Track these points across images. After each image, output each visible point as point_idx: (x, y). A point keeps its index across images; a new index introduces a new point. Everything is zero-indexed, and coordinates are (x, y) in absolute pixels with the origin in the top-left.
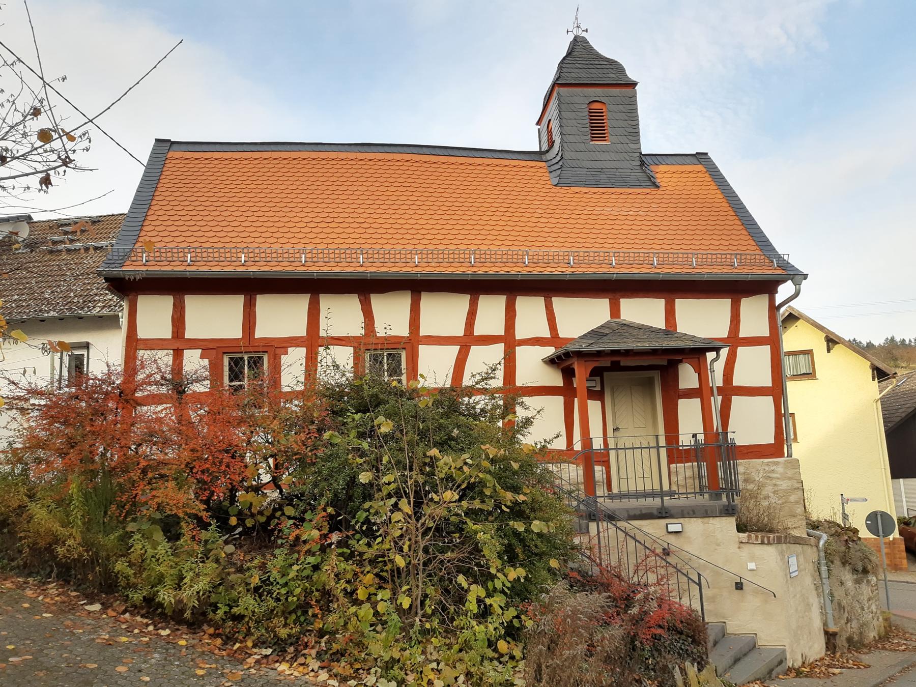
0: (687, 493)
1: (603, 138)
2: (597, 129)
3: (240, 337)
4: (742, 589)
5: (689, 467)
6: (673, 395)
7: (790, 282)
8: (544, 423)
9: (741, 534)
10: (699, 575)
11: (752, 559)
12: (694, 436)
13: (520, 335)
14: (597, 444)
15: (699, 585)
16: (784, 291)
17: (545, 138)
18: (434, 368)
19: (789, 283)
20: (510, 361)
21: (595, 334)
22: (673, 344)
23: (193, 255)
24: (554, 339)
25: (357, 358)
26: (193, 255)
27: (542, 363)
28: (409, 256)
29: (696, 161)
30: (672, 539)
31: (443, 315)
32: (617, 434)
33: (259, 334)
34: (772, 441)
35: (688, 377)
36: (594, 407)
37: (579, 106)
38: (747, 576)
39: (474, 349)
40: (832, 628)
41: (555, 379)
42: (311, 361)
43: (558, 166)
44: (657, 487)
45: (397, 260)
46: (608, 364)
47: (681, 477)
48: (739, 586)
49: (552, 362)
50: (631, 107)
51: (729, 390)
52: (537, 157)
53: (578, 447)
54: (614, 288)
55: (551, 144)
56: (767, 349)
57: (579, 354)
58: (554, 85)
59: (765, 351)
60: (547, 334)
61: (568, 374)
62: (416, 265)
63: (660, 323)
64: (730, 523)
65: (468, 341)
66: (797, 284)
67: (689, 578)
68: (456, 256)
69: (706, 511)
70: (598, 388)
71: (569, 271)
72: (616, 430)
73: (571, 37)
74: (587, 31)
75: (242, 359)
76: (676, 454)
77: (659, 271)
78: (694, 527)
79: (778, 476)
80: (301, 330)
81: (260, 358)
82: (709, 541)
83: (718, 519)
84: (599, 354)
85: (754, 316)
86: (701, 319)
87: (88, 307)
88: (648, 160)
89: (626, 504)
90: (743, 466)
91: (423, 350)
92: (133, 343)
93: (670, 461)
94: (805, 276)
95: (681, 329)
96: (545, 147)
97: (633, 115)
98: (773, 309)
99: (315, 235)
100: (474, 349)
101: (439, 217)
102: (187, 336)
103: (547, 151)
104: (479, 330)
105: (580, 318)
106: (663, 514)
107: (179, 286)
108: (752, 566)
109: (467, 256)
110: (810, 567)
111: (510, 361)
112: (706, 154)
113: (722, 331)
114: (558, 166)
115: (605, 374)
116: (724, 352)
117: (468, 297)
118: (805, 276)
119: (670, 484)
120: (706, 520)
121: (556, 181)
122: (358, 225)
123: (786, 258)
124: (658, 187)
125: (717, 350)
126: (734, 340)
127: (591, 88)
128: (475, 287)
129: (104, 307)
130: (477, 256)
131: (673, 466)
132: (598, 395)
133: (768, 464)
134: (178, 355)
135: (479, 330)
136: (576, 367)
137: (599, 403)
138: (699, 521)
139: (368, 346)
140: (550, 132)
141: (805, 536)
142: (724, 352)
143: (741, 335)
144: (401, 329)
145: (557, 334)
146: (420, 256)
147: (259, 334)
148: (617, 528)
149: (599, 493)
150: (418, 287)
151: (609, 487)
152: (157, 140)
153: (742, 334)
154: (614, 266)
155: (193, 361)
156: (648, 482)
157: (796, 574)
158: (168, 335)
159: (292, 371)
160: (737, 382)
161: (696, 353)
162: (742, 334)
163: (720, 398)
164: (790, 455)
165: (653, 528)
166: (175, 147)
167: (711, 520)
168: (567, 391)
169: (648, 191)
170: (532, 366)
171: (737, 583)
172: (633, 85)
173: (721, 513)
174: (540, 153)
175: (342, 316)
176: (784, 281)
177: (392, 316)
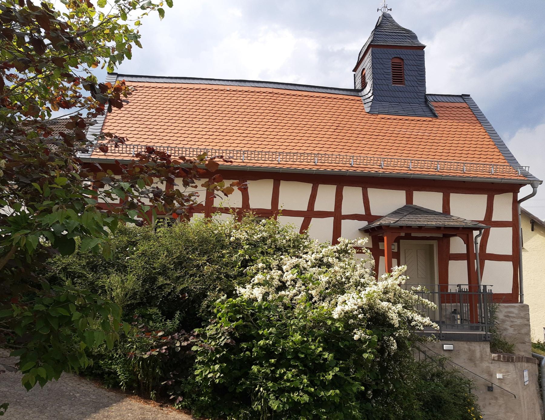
1: (401, 82)
4: (492, 391)
6: (446, 257)
12: (459, 286)
13: (344, 212)
17: (359, 81)
19: (529, 187)
20: (210, 197)
24: (368, 216)
27: (358, 231)
29: (462, 100)
31: (295, 197)
35: (457, 245)
39: (313, 220)
45: (274, 159)
49: (365, 231)
51: (485, 256)
56: (510, 230)
57: (388, 228)
60: (362, 212)
65: (309, 215)
66: (534, 187)
71: (381, 171)
73: (380, 14)
74: (391, 10)
86: (467, 209)
88: (430, 98)
96: (359, 87)
97: (421, 68)
99: (198, 140)
100: (313, 220)
101: (286, 131)
104: (317, 207)
105: (386, 203)
111: (210, 197)
112: (469, 95)
113: (481, 216)
117: (312, 185)
118: (541, 182)
126: (489, 222)
128: (315, 179)
135: (317, 207)
140: (363, 77)
145: (370, 213)
153: (494, 219)
161: (465, 231)
162: (494, 219)
164: (522, 302)
168: (376, 252)
174: (355, 90)
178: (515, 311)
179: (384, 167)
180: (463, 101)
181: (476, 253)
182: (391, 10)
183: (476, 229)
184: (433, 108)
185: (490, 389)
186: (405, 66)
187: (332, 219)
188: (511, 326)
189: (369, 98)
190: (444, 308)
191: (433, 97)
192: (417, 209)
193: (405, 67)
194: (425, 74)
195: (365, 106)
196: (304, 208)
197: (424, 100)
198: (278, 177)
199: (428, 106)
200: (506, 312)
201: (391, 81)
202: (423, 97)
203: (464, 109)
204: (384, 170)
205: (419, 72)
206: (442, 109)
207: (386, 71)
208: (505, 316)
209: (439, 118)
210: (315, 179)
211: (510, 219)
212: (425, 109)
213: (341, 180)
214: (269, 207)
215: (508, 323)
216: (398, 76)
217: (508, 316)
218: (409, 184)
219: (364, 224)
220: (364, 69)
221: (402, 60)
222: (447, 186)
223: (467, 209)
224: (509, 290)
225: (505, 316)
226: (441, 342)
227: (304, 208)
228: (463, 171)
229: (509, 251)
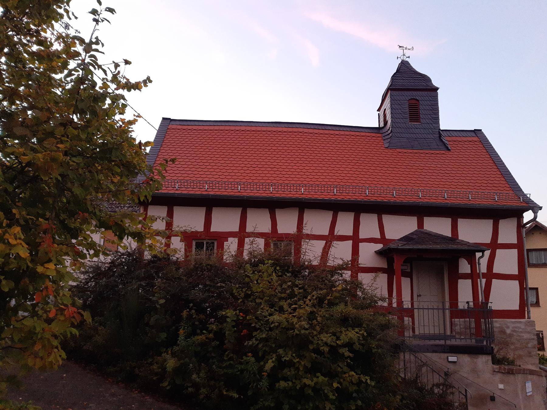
2: (414, 116)
3: (203, 230)
4: (494, 400)
6: (455, 276)
7: (530, 211)
8: (375, 285)
10: (466, 390)
12: (468, 303)
13: (362, 236)
14: (407, 305)
16: (528, 216)
19: (530, 212)
20: (355, 251)
21: (407, 239)
22: (455, 247)
23: (180, 184)
24: (383, 239)
25: (267, 245)
26: (180, 184)
28: (298, 188)
30: (451, 367)
31: (317, 223)
32: (419, 298)
33: (213, 229)
34: (517, 308)
35: (464, 267)
36: (405, 282)
37: (402, 102)
38: (497, 394)
41: (382, 264)
42: (241, 245)
43: (389, 137)
44: (442, 332)
50: (433, 102)
51: (490, 275)
52: (376, 131)
53: (395, 305)
54: (420, 211)
55: (386, 123)
56: (515, 251)
58: (388, 90)
59: (514, 252)
60: (378, 236)
61: (390, 262)
62: (303, 193)
63: (447, 232)
64: (489, 358)
65: (331, 238)
68: (326, 189)
70: (409, 270)
72: (419, 296)
73: (399, 61)
74: (409, 57)
77: (448, 201)
79: (521, 330)
80: (235, 227)
81: (213, 243)
85: (508, 233)
86: (474, 232)
87: (121, 207)
89: (421, 343)
90: (498, 323)
93: (452, 317)
94: (541, 208)
95: (460, 238)
96: (382, 125)
97: (436, 107)
103: (383, 128)
105: (399, 228)
107: (171, 202)
109: (332, 189)
111: (355, 251)
112: (481, 130)
113: (487, 239)
116: (487, 253)
117: (332, 212)
118: (541, 208)
121: (387, 145)
122: (271, 169)
123: (528, 196)
124: (449, 150)
125: (483, 251)
127: (411, 92)
128: (335, 207)
129: (129, 207)
130: (338, 189)
132: (409, 275)
136: (395, 257)
139: (273, 237)
141: (538, 369)
142: (487, 253)
143: (499, 242)
146: (305, 188)
147: (213, 229)
149: (406, 334)
150: (302, 206)
152: (164, 119)
153: (500, 241)
154: (421, 196)
155: (177, 243)
156: (432, 328)
157: (531, 394)
160: (496, 270)
161: (470, 252)
162: (500, 241)
163: (484, 281)
164: (529, 318)
165: (437, 359)
166: (172, 123)
168: (389, 271)
169: (444, 152)
170: (368, 254)
171: (491, 397)
172: (437, 89)
175: (259, 222)
177: (287, 224)
181: (479, 273)
182: (409, 57)
183: (479, 251)
184: (446, 142)
185: (493, 399)
186: (421, 106)
187: (351, 242)
189: (389, 134)
191: (448, 132)
192: (426, 233)
194: (438, 113)
195: (385, 142)
196: (499, 252)
197: (438, 135)
199: (442, 141)
200: (513, 327)
201: (408, 120)
203: (476, 143)
206: (455, 143)
209: (452, 151)
211: (515, 242)
218: (420, 211)
220: (385, 109)
223: (474, 232)
224: (515, 306)
226: (446, 355)
227: (326, 233)
228: (469, 198)
229: (515, 271)
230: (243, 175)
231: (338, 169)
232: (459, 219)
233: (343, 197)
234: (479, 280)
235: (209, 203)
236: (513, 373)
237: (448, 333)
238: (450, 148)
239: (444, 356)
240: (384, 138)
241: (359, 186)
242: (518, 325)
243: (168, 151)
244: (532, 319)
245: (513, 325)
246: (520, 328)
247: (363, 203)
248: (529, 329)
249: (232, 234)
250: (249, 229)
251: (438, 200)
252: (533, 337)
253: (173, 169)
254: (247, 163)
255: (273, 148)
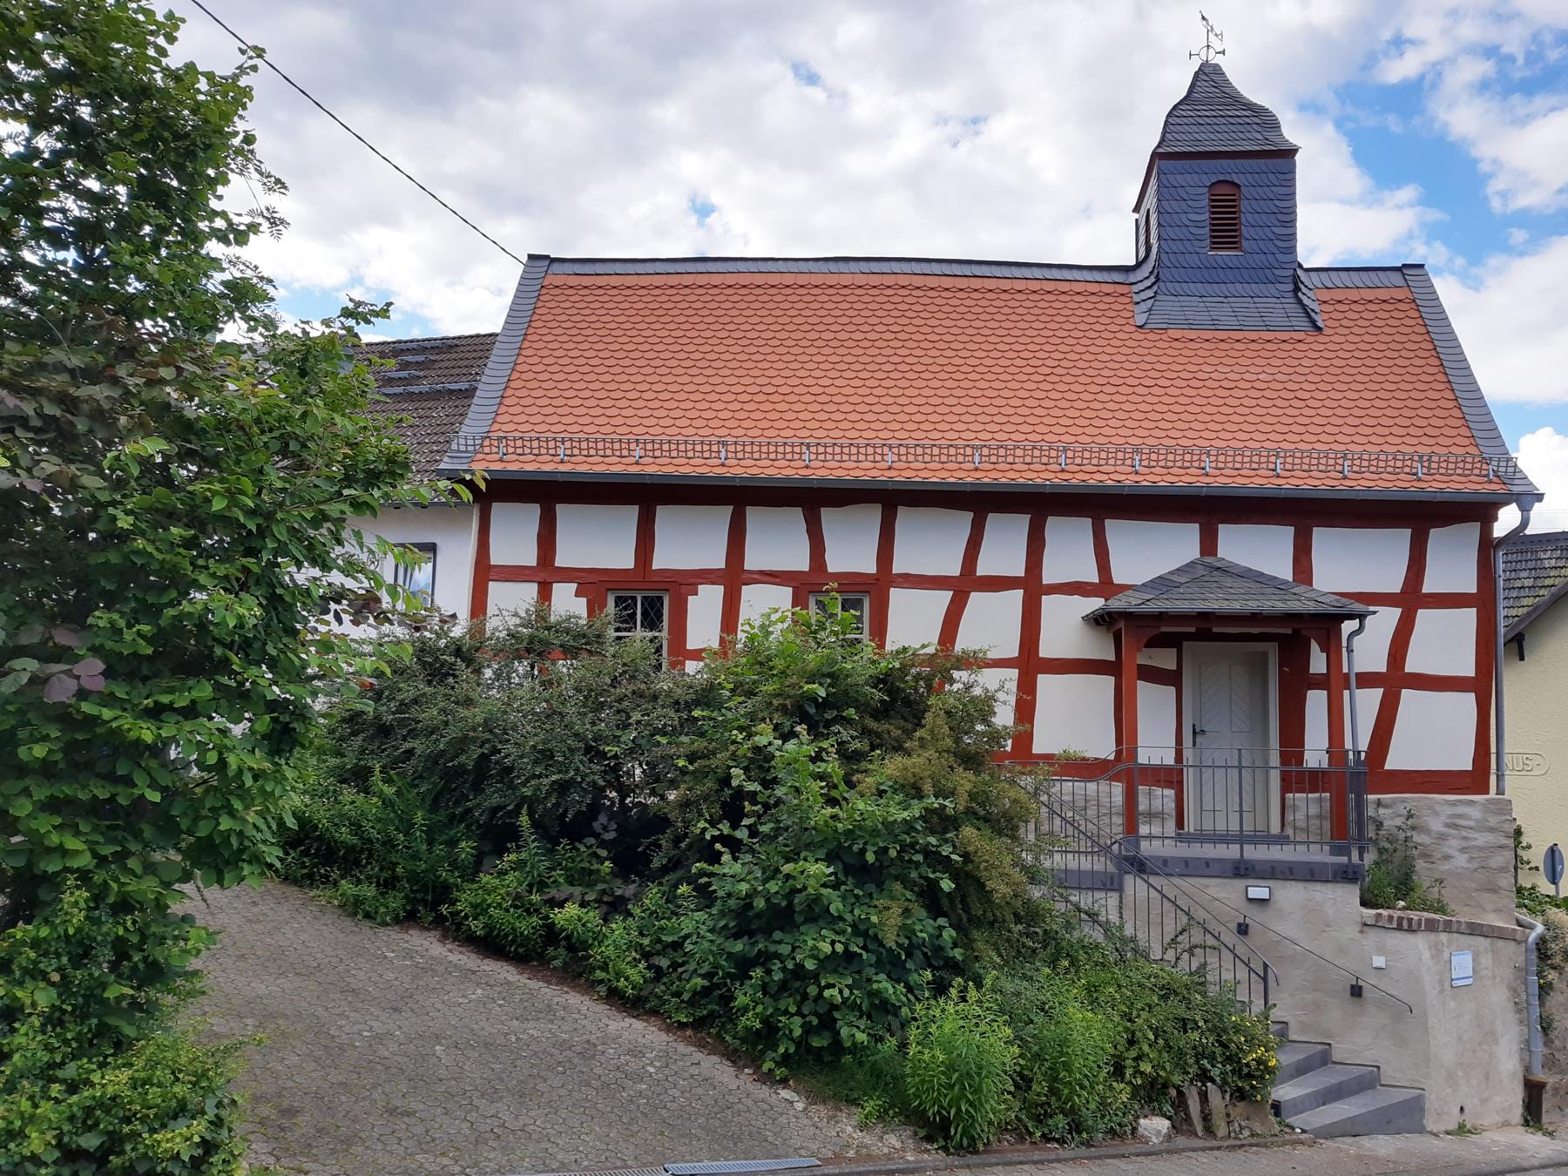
0: (1308, 843)
1: (1234, 244)
5: (1314, 800)
6: (1296, 685)
8: (1072, 718)
9: (1365, 911)
10: (1266, 966)
11: (1381, 951)
13: (1048, 578)
15: (1265, 979)
16: (1507, 520)
18: (913, 622)
31: (931, 546)
33: (658, 563)
38: (1369, 981)
39: (975, 597)
40: (1539, 1075)
41: (1100, 648)
43: (1150, 293)
46: (1193, 630)
47: (1300, 815)
48: (1356, 991)
49: (1099, 620)
51: (1395, 680)
54: (1209, 510)
56: (1470, 614)
59: (1468, 618)
60: (1093, 577)
65: (964, 585)
67: (1251, 969)
69: (1312, 871)
75: (634, 599)
76: (1297, 778)
78: (1291, 894)
79: (1472, 823)
80: (718, 561)
81: (660, 599)
82: (1318, 920)
83: (1329, 886)
84: (1162, 617)
85: (1452, 564)
86: (1353, 564)
91: (897, 596)
92: (485, 572)
93: (1286, 787)
98: (1488, 546)
102: (557, 564)
104: (984, 568)
105: (1149, 557)
106: (1242, 870)
108: (1379, 961)
110: (1508, 973)
112: (1422, 266)
113: (1393, 582)
114: (1150, 293)
115: (1185, 644)
117: (969, 516)
119: (1283, 825)
120: (1311, 886)
121: (1140, 320)
124: (1319, 329)
131: (1289, 795)
133: (1454, 804)
134: (545, 594)
135: (984, 568)
137: (1173, 689)
138: (1301, 885)
144: (867, 564)
147: (658, 563)
148: (1150, 885)
151: (1180, 823)
152: (531, 257)
158: (532, 561)
159: (703, 617)
160: (1412, 665)
162: (1428, 587)
164: (1500, 791)
165: (1225, 895)
166: (556, 268)
167: (1319, 886)
169: (1301, 336)
170: (1065, 627)
172: (1290, 152)
173: (1335, 876)
175: (777, 543)
176: (1507, 503)
177: (851, 549)
178: (1475, 813)
179: (1142, 470)
180: (1402, 283)
183: (1351, 617)
187: (1018, 595)
188: (1463, 850)
190: (1289, 803)
193: (1244, 206)
194: (1294, 220)
195: (1137, 309)
197: (1291, 287)
198: (891, 500)
199: (1300, 302)
200: (1450, 816)
202: (1290, 280)
204: (1138, 478)
205: (1281, 217)
207: (1193, 217)
208: (1447, 825)
210: (980, 503)
212: (1293, 308)
213: (1040, 505)
214: (871, 568)
215: (1455, 843)
216: (1225, 230)
217: (1455, 826)
218: (1209, 510)
219: (1096, 603)
221: (1238, 186)
222: (1304, 513)
224: (1463, 761)
225: (1447, 825)
227: (954, 569)
230: (737, 415)
231: (1075, 396)
232: (558, 507)
233: (1034, 475)
234: (1346, 693)
235: (647, 496)
236: (1411, 930)
237: (1275, 828)
238: (1320, 324)
239: (1240, 884)
240: (1137, 298)
241: (1404, 454)
242: (1461, 810)
243: (541, 353)
244: (1506, 797)
245: (1450, 811)
246: (1469, 818)
247: (1048, 490)
248: (1493, 821)
249: (707, 576)
250: (752, 562)
251: (1452, 485)
252: (1504, 841)
253: (554, 402)
254: (798, 381)
255: (823, 335)
